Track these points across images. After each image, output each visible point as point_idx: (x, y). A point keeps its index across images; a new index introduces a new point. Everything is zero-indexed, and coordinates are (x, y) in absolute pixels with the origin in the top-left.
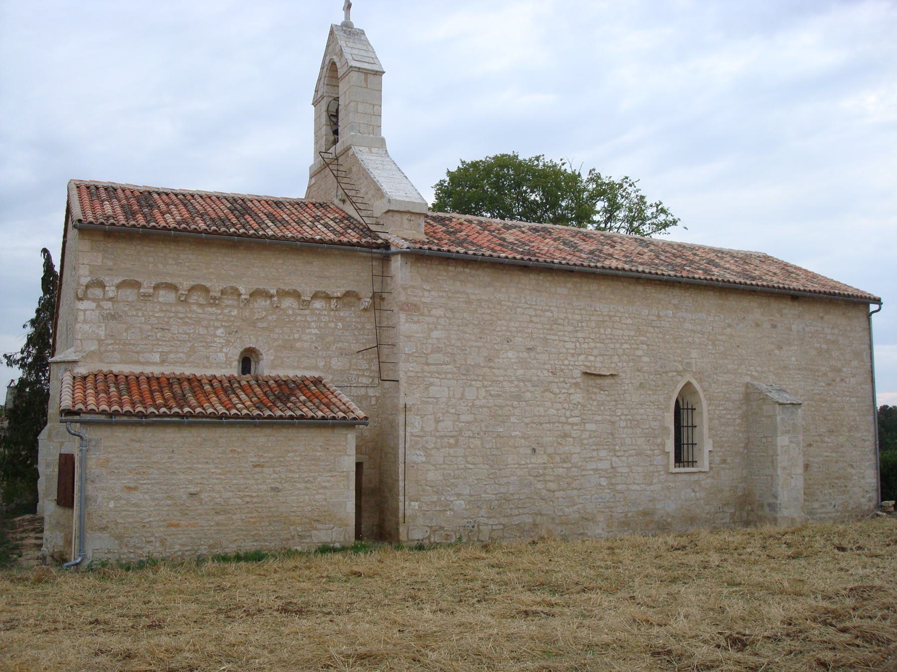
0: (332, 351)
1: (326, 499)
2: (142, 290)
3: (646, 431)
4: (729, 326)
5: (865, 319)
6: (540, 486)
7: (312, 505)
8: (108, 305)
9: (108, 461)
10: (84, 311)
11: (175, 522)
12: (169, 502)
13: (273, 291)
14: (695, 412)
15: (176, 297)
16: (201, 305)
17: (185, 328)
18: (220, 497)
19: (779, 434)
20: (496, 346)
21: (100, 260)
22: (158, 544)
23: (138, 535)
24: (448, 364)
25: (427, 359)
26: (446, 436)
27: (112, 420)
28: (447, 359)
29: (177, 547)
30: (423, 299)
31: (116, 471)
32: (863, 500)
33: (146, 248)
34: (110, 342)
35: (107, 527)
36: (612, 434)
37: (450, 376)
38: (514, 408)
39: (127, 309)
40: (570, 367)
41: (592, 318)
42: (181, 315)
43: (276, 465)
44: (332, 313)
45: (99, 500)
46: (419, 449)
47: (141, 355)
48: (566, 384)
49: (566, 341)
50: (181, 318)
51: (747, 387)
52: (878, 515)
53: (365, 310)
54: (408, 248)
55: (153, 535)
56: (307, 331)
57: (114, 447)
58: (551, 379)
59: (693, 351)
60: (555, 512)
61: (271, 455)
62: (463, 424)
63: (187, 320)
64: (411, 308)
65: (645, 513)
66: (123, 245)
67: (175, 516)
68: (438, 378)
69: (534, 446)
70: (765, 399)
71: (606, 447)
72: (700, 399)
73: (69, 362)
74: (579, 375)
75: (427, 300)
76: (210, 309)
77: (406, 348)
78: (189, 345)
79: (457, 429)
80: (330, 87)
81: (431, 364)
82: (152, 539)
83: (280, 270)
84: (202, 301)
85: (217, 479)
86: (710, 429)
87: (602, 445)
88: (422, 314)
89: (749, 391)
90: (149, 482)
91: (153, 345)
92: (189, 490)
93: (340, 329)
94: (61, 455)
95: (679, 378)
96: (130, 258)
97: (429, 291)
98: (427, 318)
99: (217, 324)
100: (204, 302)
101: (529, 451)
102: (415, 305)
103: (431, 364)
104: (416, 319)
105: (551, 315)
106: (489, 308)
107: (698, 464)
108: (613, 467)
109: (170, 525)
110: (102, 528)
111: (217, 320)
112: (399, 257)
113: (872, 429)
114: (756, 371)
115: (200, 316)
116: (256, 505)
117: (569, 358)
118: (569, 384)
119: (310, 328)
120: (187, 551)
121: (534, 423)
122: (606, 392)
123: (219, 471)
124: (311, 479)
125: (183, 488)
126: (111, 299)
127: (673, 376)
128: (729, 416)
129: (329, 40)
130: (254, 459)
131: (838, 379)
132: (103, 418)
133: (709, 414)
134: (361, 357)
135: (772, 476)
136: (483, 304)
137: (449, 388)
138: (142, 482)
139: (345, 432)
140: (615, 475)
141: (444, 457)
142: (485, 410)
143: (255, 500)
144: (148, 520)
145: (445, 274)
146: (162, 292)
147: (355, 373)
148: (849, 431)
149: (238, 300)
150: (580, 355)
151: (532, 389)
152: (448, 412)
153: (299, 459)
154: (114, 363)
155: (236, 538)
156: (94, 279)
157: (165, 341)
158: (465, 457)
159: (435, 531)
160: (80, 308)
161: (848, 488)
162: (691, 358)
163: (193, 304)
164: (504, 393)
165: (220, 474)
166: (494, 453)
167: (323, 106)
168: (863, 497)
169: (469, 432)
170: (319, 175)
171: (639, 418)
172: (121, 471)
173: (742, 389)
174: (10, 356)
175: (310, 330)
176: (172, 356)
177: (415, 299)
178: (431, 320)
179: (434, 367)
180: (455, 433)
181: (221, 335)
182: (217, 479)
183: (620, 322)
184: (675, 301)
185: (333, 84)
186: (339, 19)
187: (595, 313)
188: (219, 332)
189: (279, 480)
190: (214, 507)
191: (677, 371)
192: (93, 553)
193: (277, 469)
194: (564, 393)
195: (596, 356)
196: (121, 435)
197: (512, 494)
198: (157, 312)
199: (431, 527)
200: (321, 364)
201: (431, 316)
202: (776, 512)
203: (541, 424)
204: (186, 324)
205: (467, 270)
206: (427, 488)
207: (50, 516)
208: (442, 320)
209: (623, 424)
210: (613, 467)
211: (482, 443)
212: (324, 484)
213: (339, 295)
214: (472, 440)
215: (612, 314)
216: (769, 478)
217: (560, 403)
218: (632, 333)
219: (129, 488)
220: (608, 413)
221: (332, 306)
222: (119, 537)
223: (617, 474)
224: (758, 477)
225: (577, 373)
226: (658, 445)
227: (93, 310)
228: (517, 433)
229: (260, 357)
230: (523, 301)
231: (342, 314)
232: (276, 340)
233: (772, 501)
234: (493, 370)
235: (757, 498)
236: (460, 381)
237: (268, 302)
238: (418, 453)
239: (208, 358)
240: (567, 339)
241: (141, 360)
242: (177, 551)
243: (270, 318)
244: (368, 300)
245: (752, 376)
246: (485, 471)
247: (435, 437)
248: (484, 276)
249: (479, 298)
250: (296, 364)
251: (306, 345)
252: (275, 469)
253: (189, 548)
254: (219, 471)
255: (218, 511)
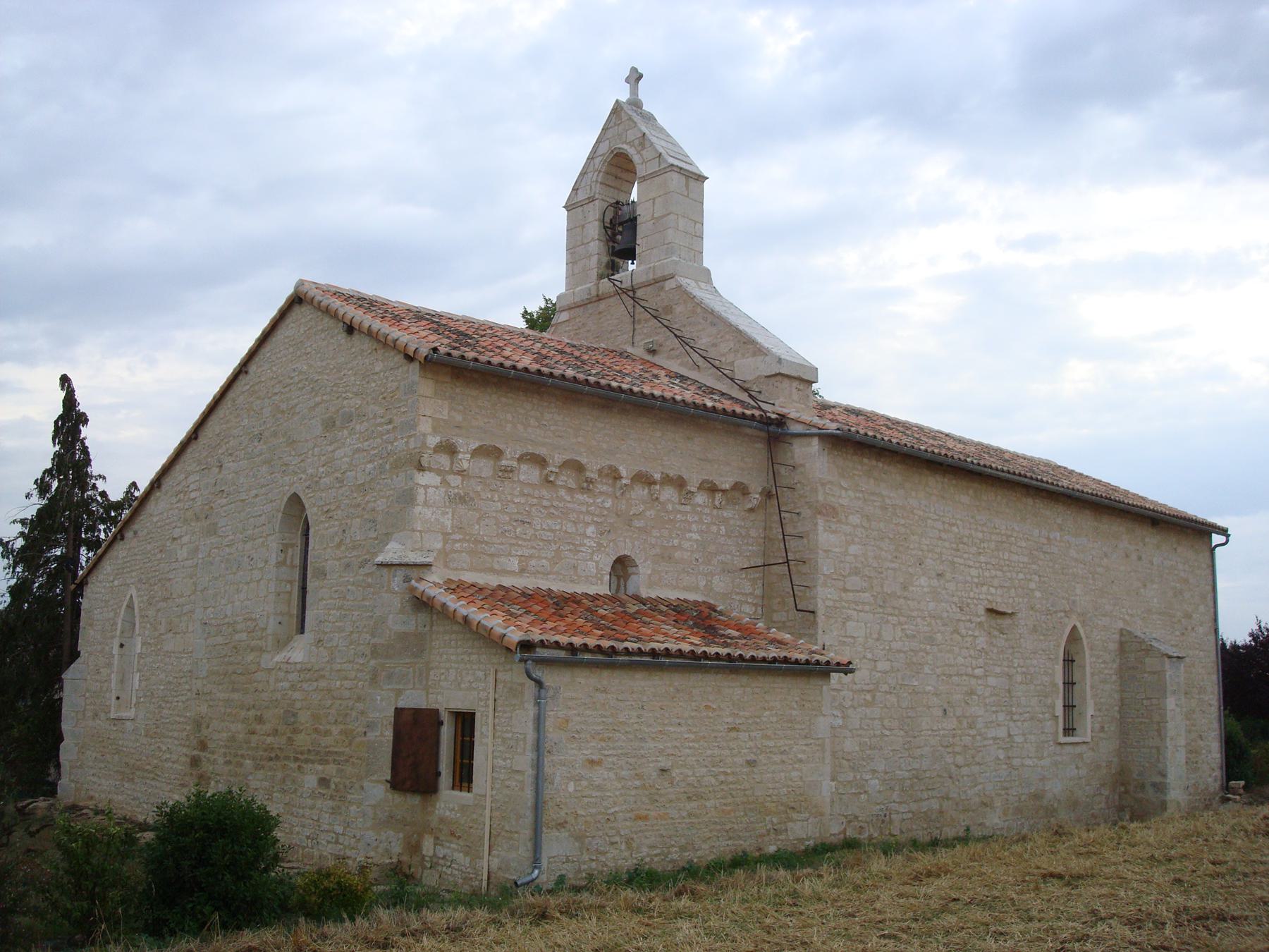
0: (714, 565)
1: (801, 778)
2: (504, 462)
3: (1038, 688)
4: (1106, 555)
5: (1207, 554)
6: (949, 760)
7: (788, 787)
8: (455, 481)
9: (567, 721)
10: (426, 487)
11: (644, 813)
12: (638, 783)
13: (657, 476)
14: (1074, 663)
15: (541, 474)
16: (570, 490)
17: (550, 522)
18: (694, 775)
19: (1168, 694)
20: (910, 570)
21: (446, 412)
22: (623, 847)
23: (600, 833)
24: (863, 591)
25: (845, 583)
26: (863, 691)
27: (574, 657)
28: (865, 584)
29: (645, 850)
30: (840, 501)
31: (576, 736)
32: (1210, 780)
33: (504, 400)
34: (457, 537)
35: (566, 822)
36: (1009, 691)
37: (867, 608)
38: (927, 653)
39: (479, 488)
40: (975, 601)
41: (993, 537)
42: (545, 503)
43: (752, 728)
44: (715, 512)
45: (557, 780)
46: (836, 708)
47: (496, 559)
48: (972, 623)
49: (971, 567)
50: (545, 507)
51: (1122, 635)
52: (1229, 799)
53: (751, 510)
54: (838, 429)
55: (618, 832)
56: (687, 535)
57: (576, 699)
58: (958, 616)
59: (1078, 586)
60: (959, 794)
61: (747, 714)
62: (880, 674)
63: (552, 510)
64: (830, 511)
65: (1036, 797)
66: (474, 393)
67: (643, 803)
68: (855, 609)
69: (946, 706)
70: (1149, 650)
71: (1004, 708)
72: (1083, 648)
73: (415, 565)
74: (983, 613)
75: (845, 502)
76: (580, 497)
77: (826, 567)
78: (554, 547)
79: (874, 682)
80: (604, 187)
81: (848, 591)
82: (617, 839)
83: (659, 447)
84: (572, 484)
85: (690, 748)
86: (1092, 687)
87: (1000, 706)
88: (839, 521)
89: (1123, 639)
90: (614, 752)
91: (512, 545)
92: (660, 764)
93: (723, 536)
94: (399, 712)
95: (1066, 620)
96: (483, 412)
97: (846, 490)
98: (844, 527)
99: (588, 519)
100: (574, 486)
101: (940, 713)
102: (834, 508)
103: (848, 591)
104: (834, 527)
105: (957, 530)
106: (903, 518)
107: (1078, 731)
108: (1010, 735)
109: (639, 818)
110: (559, 824)
111: (588, 512)
112: (815, 441)
113: (1216, 692)
114: (1128, 614)
115: (568, 505)
116: (731, 786)
117: (975, 589)
118: (974, 624)
119: (690, 531)
120: (656, 855)
121: (944, 675)
122: (1005, 636)
123: (692, 736)
124: (787, 748)
125: (653, 761)
126: (461, 473)
127: (1061, 618)
128: (1106, 671)
129: (609, 120)
130: (730, 720)
131: (1190, 628)
132: (562, 654)
133: (1091, 668)
134: (744, 576)
135: (1158, 748)
136: (898, 511)
137: (866, 624)
138: (606, 752)
139: (821, 683)
140: (1012, 746)
141: (861, 718)
142: (902, 655)
143: (730, 779)
144: (613, 810)
145: (860, 467)
146: (524, 467)
147: (738, 598)
148: (1199, 693)
149: (614, 486)
150: (983, 585)
151: (942, 629)
152: (864, 657)
153: (774, 719)
154: (463, 569)
155: (708, 835)
156: (444, 439)
157: (525, 540)
158: (881, 719)
159: (850, 822)
160: (421, 482)
161: (1199, 765)
162: (1076, 595)
163: (561, 486)
164: (918, 632)
165: (693, 741)
166: (909, 714)
167: (593, 215)
168: (1210, 776)
169: (886, 685)
170: (579, 311)
171: (1032, 670)
172: (582, 735)
173: (1117, 637)
174: (8, 542)
175: (691, 534)
176: (533, 562)
177: (833, 499)
178: (848, 529)
179: (851, 594)
180: (872, 687)
181: (591, 535)
182: (690, 748)
183: (1015, 544)
184: (1059, 521)
185: (607, 183)
186: (624, 96)
187: (995, 531)
188: (590, 530)
189: (754, 750)
190: (686, 789)
191: (1065, 612)
192: (549, 863)
193: (753, 734)
194: (970, 636)
195: (996, 588)
196: (583, 682)
197: (925, 771)
198: (517, 496)
199: (846, 817)
200: (702, 583)
201: (847, 524)
202: (1166, 795)
203: (951, 676)
204: (551, 516)
205: (880, 465)
206: (844, 762)
207: (374, 806)
208: (859, 529)
209: (1019, 678)
210: (1010, 735)
211: (898, 701)
212: (800, 756)
213: (727, 486)
214: (888, 696)
215: (1009, 533)
216: (1154, 751)
217: (967, 648)
218: (1026, 560)
219: (592, 762)
220: (1005, 663)
221: (717, 503)
222: (579, 838)
223: (1015, 745)
224: (1136, 750)
225: (981, 611)
226: (1048, 707)
227: (437, 487)
228: (930, 688)
229: (630, 570)
230: (933, 510)
231: (725, 514)
232: (653, 546)
233: (1158, 779)
234: (909, 602)
235: (1135, 776)
236: (878, 615)
237: (646, 491)
238: (835, 713)
239: (575, 567)
240: (971, 563)
241: (496, 567)
242: (645, 857)
243: (648, 513)
244: (757, 496)
245: (1124, 620)
246: (901, 739)
247: (852, 691)
248: (895, 473)
249: (894, 503)
250: (674, 584)
251: (686, 555)
252: (751, 733)
253: (658, 851)
254: (692, 736)
255: (691, 795)
